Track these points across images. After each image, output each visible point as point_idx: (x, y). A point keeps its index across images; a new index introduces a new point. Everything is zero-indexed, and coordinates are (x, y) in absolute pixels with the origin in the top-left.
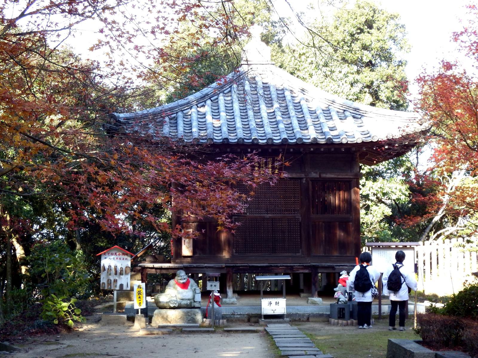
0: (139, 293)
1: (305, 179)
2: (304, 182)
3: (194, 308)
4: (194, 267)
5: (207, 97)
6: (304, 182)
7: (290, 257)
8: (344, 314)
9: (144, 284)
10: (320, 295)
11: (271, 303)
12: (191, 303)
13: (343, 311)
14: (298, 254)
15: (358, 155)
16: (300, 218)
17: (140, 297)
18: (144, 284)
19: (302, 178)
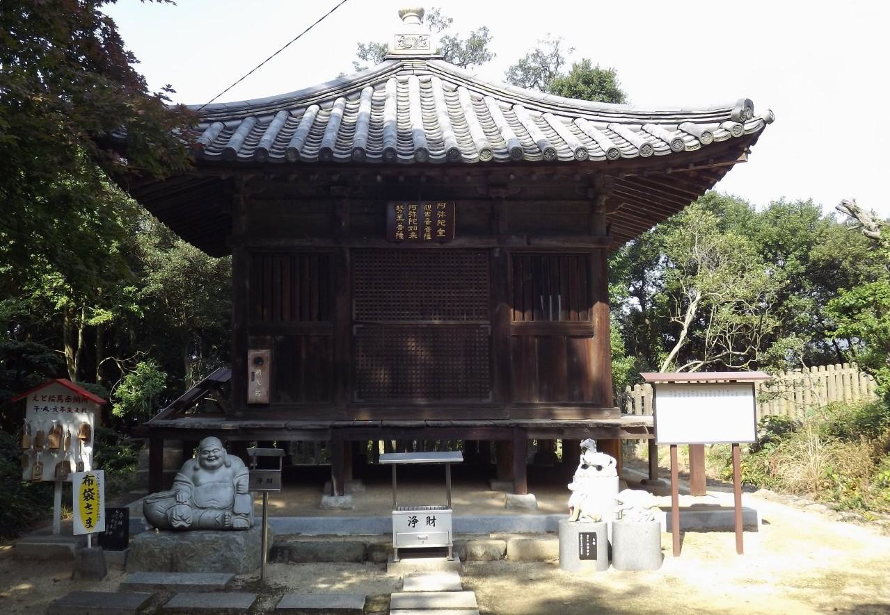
0: (88, 495)
1: (498, 250)
2: (497, 255)
3: (232, 529)
4: (262, 429)
5: (315, 100)
6: (497, 255)
7: (349, 520)
8: (594, 549)
9: (102, 472)
10: (475, 442)
11: (415, 521)
12: (224, 517)
13: (591, 542)
14: (485, 401)
15: (604, 200)
16: (489, 327)
17: (88, 506)
18: (102, 472)
19: (494, 248)
